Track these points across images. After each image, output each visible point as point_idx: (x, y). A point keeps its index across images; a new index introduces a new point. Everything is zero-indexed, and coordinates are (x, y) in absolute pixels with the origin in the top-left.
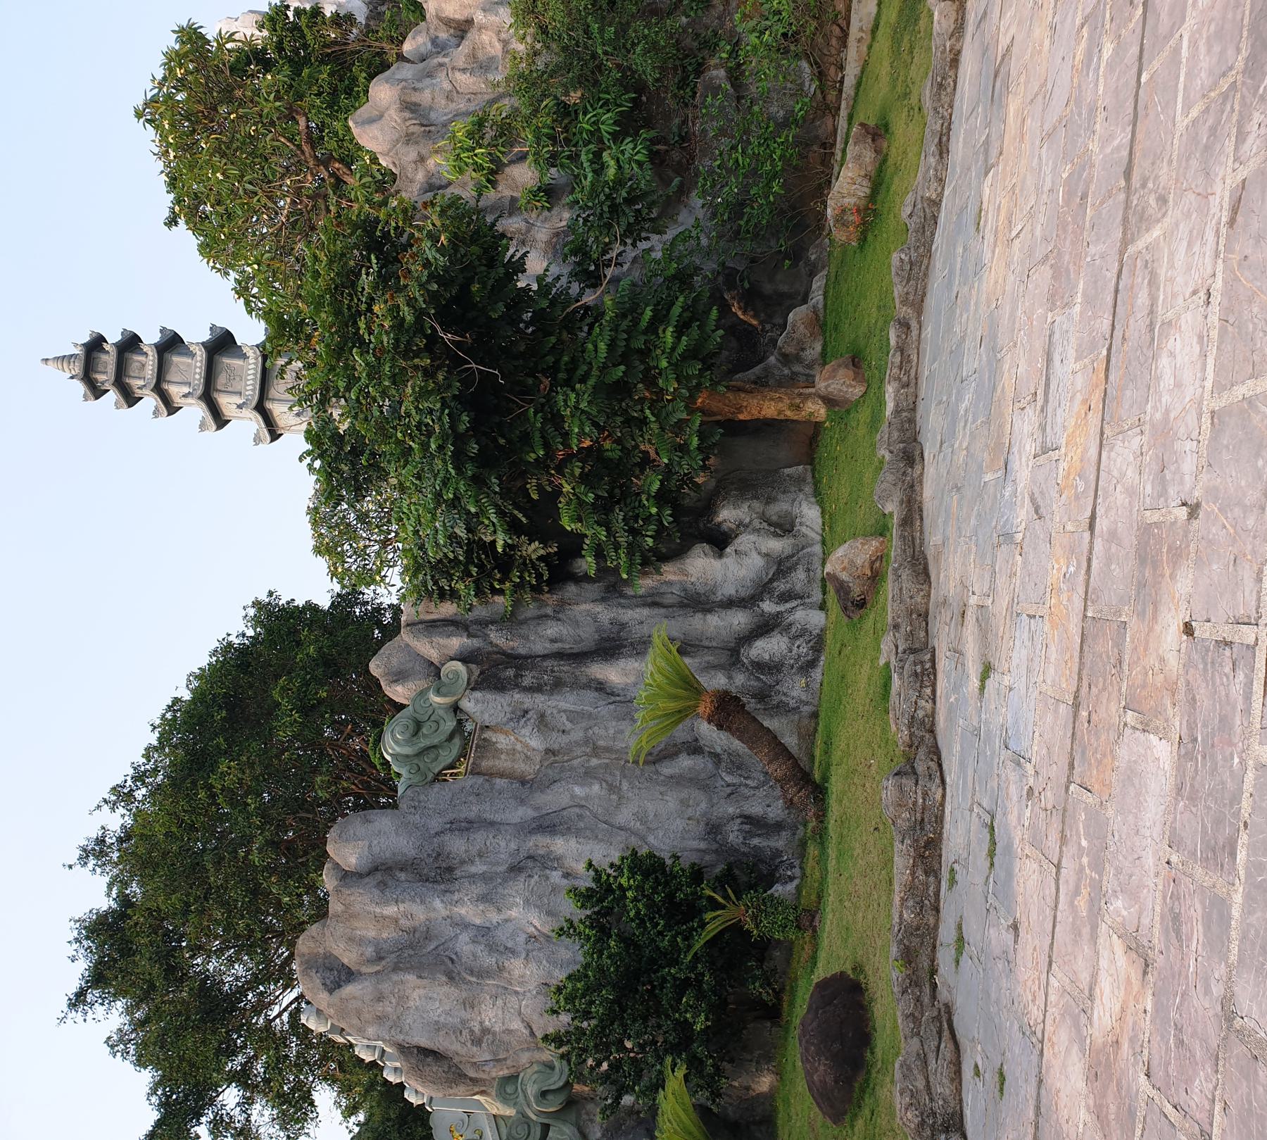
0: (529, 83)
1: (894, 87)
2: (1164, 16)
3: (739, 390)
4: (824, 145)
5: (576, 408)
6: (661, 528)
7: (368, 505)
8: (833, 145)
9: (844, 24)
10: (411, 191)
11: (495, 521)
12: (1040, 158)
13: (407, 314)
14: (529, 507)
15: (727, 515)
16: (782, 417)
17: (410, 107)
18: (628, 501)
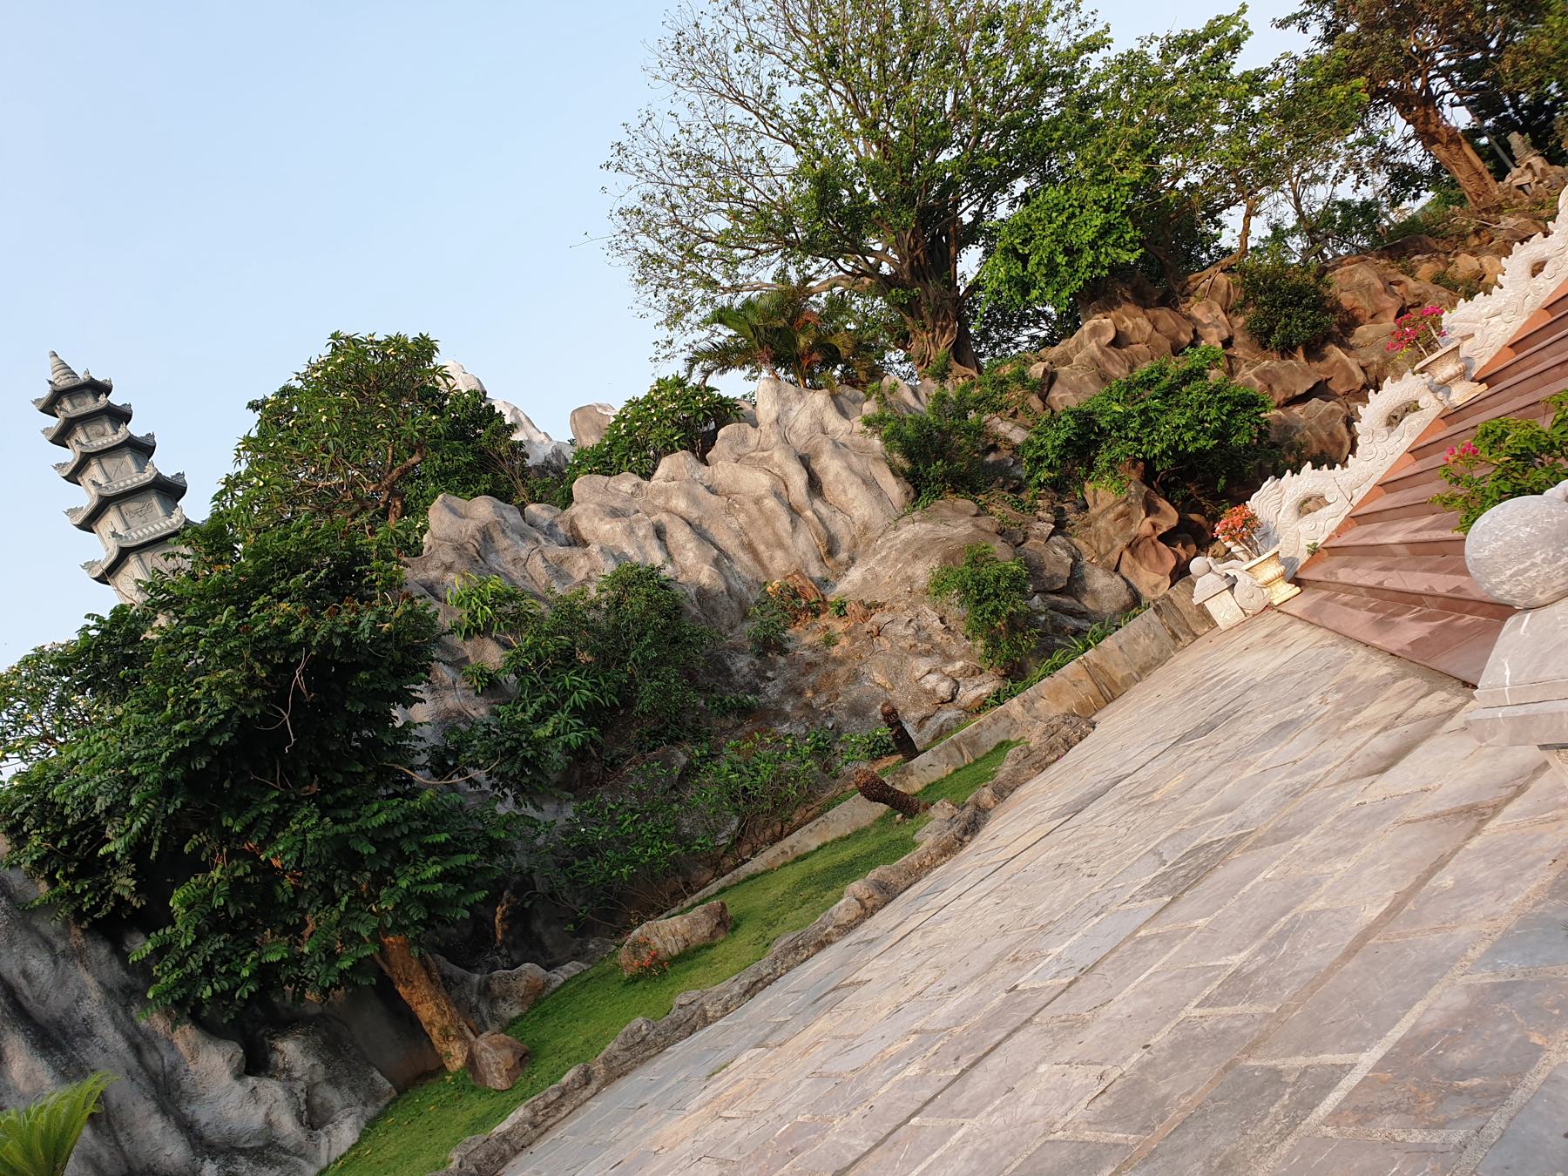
0: (570, 615)
1: (770, 909)
2: (966, 1096)
3: (427, 968)
4: (687, 884)
5: (304, 832)
6: (227, 995)
7: (81, 701)
8: (693, 893)
9: (786, 831)
10: (413, 574)
11: (134, 829)
12: (799, 1083)
13: (296, 634)
14: (172, 851)
15: (290, 1050)
16: (427, 1029)
17: (486, 535)
18: (240, 942)
